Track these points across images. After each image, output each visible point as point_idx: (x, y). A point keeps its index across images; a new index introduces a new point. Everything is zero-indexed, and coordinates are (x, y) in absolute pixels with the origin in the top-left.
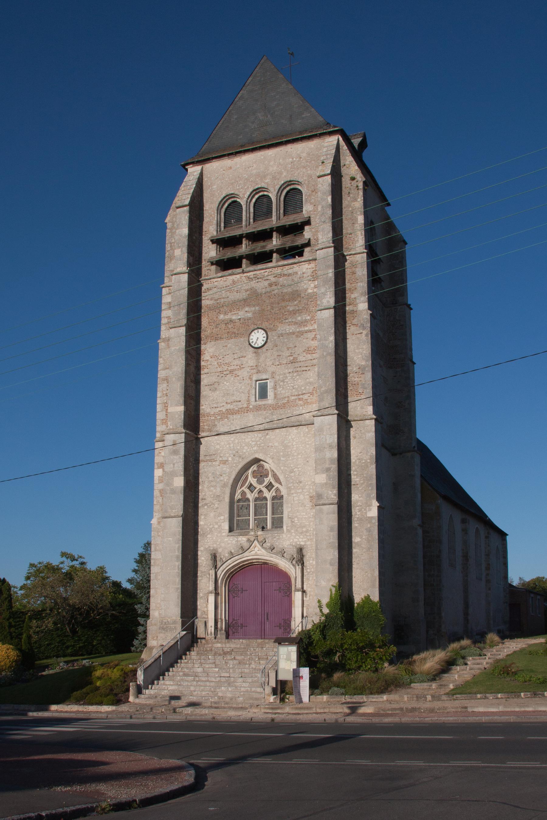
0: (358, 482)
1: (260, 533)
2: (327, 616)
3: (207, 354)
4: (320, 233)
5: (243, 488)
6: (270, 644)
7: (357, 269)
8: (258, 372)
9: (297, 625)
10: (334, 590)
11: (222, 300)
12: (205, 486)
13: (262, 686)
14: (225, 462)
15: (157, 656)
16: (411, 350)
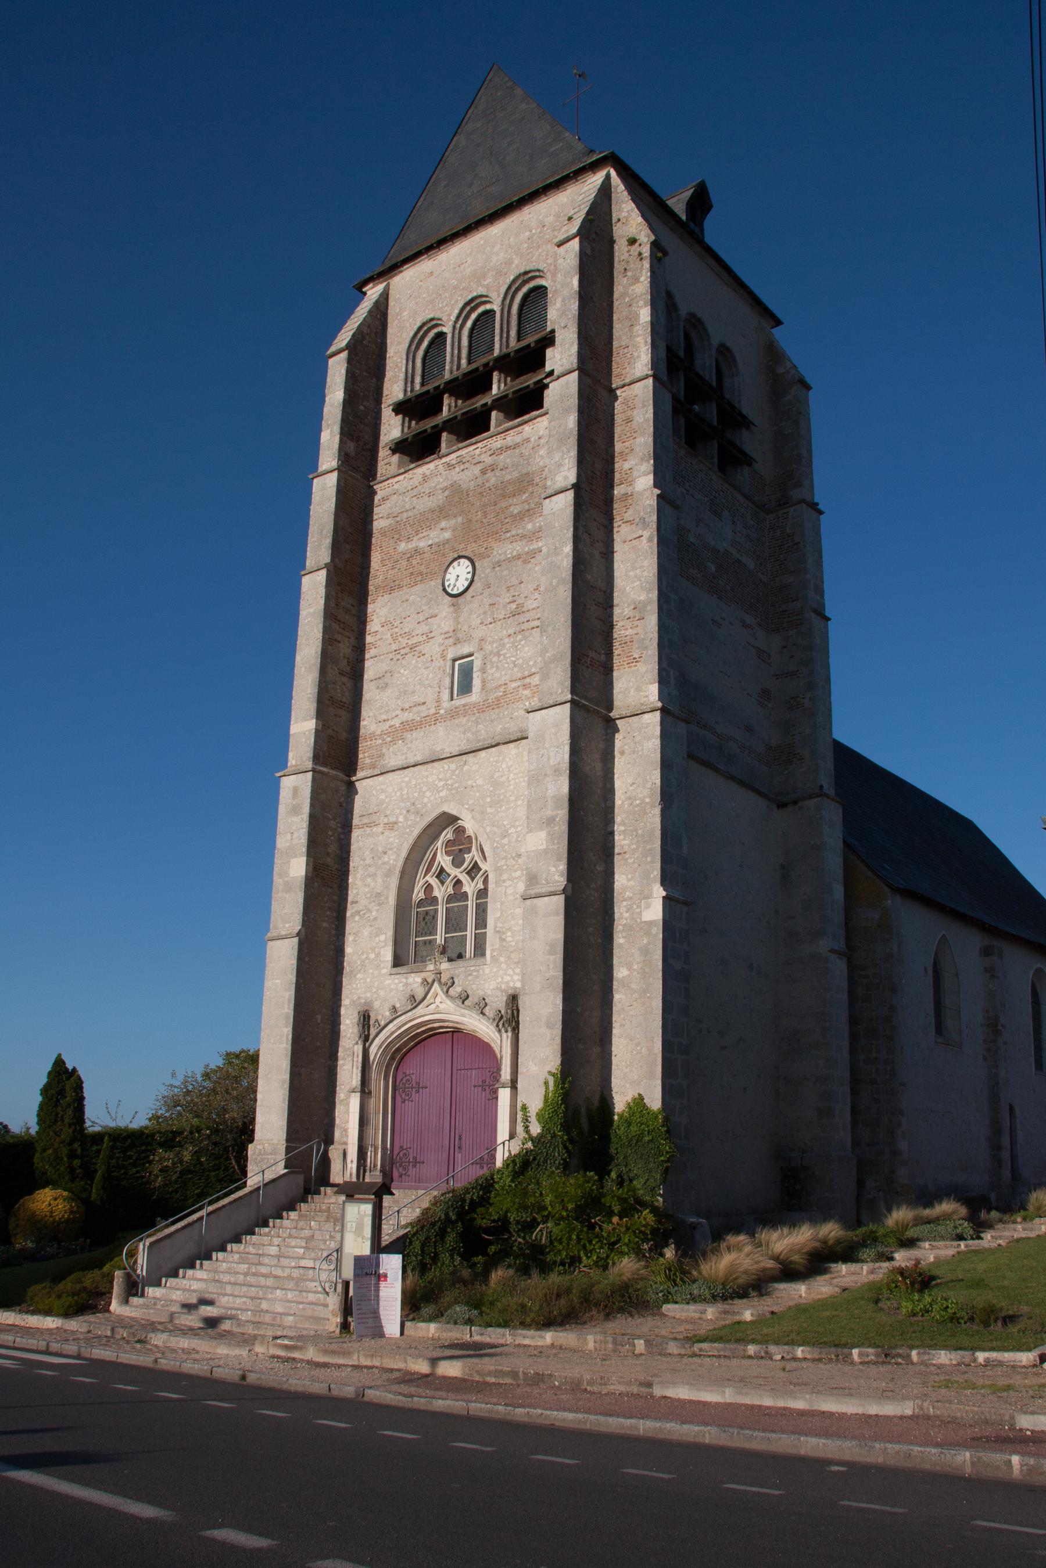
0: (626, 848)
2: (537, 1141)
3: (376, 621)
5: (428, 878)
7: (635, 412)
8: (457, 642)
10: (551, 1081)
11: (405, 515)
12: (359, 876)
14: (391, 826)
16: (820, 591)
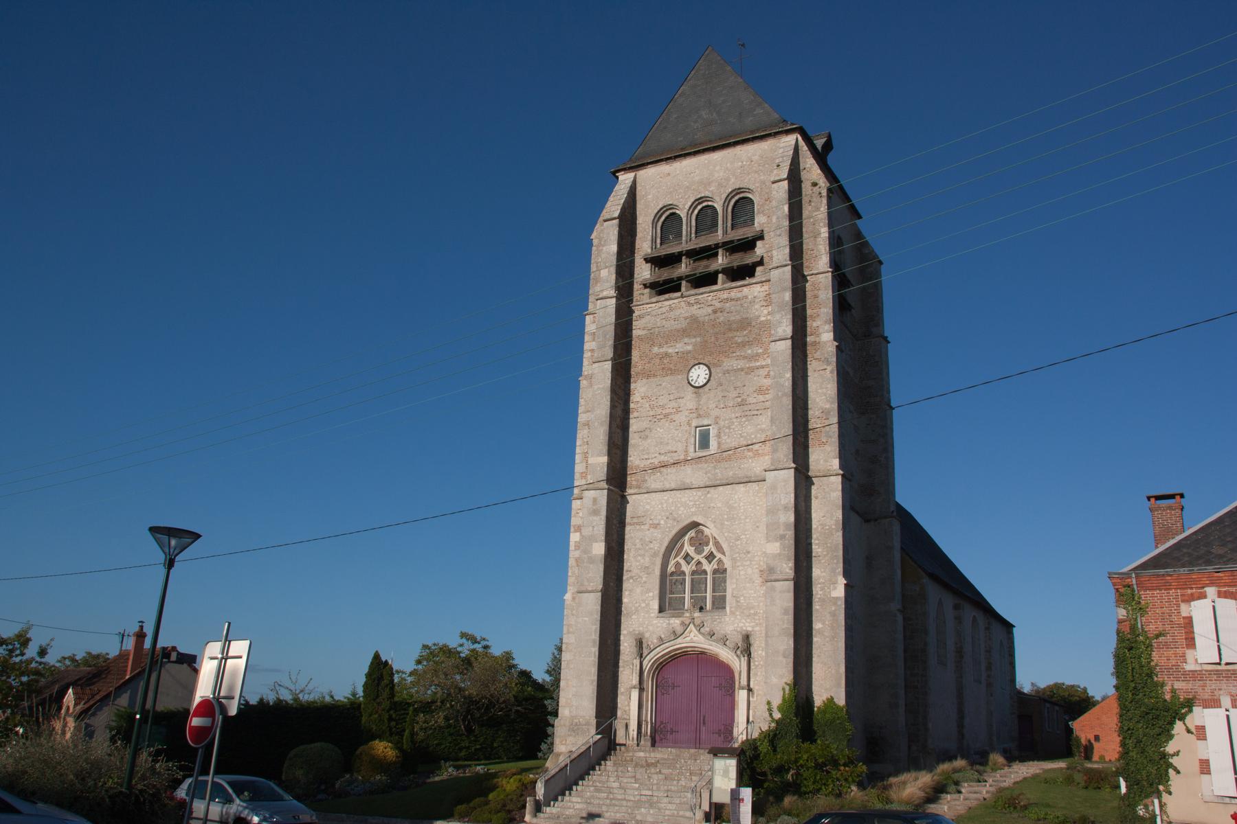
1: (697, 614)
2: (778, 722)
4: (774, 249)
6: (705, 756)
8: (699, 416)
9: (741, 732)
10: (787, 688)
13: (692, 809)
14: (656, 526)
15: (563, 764)
16: (889, 392)
